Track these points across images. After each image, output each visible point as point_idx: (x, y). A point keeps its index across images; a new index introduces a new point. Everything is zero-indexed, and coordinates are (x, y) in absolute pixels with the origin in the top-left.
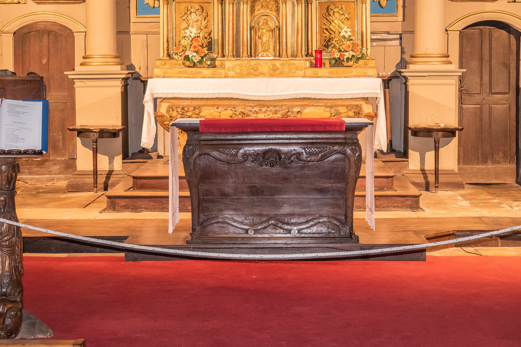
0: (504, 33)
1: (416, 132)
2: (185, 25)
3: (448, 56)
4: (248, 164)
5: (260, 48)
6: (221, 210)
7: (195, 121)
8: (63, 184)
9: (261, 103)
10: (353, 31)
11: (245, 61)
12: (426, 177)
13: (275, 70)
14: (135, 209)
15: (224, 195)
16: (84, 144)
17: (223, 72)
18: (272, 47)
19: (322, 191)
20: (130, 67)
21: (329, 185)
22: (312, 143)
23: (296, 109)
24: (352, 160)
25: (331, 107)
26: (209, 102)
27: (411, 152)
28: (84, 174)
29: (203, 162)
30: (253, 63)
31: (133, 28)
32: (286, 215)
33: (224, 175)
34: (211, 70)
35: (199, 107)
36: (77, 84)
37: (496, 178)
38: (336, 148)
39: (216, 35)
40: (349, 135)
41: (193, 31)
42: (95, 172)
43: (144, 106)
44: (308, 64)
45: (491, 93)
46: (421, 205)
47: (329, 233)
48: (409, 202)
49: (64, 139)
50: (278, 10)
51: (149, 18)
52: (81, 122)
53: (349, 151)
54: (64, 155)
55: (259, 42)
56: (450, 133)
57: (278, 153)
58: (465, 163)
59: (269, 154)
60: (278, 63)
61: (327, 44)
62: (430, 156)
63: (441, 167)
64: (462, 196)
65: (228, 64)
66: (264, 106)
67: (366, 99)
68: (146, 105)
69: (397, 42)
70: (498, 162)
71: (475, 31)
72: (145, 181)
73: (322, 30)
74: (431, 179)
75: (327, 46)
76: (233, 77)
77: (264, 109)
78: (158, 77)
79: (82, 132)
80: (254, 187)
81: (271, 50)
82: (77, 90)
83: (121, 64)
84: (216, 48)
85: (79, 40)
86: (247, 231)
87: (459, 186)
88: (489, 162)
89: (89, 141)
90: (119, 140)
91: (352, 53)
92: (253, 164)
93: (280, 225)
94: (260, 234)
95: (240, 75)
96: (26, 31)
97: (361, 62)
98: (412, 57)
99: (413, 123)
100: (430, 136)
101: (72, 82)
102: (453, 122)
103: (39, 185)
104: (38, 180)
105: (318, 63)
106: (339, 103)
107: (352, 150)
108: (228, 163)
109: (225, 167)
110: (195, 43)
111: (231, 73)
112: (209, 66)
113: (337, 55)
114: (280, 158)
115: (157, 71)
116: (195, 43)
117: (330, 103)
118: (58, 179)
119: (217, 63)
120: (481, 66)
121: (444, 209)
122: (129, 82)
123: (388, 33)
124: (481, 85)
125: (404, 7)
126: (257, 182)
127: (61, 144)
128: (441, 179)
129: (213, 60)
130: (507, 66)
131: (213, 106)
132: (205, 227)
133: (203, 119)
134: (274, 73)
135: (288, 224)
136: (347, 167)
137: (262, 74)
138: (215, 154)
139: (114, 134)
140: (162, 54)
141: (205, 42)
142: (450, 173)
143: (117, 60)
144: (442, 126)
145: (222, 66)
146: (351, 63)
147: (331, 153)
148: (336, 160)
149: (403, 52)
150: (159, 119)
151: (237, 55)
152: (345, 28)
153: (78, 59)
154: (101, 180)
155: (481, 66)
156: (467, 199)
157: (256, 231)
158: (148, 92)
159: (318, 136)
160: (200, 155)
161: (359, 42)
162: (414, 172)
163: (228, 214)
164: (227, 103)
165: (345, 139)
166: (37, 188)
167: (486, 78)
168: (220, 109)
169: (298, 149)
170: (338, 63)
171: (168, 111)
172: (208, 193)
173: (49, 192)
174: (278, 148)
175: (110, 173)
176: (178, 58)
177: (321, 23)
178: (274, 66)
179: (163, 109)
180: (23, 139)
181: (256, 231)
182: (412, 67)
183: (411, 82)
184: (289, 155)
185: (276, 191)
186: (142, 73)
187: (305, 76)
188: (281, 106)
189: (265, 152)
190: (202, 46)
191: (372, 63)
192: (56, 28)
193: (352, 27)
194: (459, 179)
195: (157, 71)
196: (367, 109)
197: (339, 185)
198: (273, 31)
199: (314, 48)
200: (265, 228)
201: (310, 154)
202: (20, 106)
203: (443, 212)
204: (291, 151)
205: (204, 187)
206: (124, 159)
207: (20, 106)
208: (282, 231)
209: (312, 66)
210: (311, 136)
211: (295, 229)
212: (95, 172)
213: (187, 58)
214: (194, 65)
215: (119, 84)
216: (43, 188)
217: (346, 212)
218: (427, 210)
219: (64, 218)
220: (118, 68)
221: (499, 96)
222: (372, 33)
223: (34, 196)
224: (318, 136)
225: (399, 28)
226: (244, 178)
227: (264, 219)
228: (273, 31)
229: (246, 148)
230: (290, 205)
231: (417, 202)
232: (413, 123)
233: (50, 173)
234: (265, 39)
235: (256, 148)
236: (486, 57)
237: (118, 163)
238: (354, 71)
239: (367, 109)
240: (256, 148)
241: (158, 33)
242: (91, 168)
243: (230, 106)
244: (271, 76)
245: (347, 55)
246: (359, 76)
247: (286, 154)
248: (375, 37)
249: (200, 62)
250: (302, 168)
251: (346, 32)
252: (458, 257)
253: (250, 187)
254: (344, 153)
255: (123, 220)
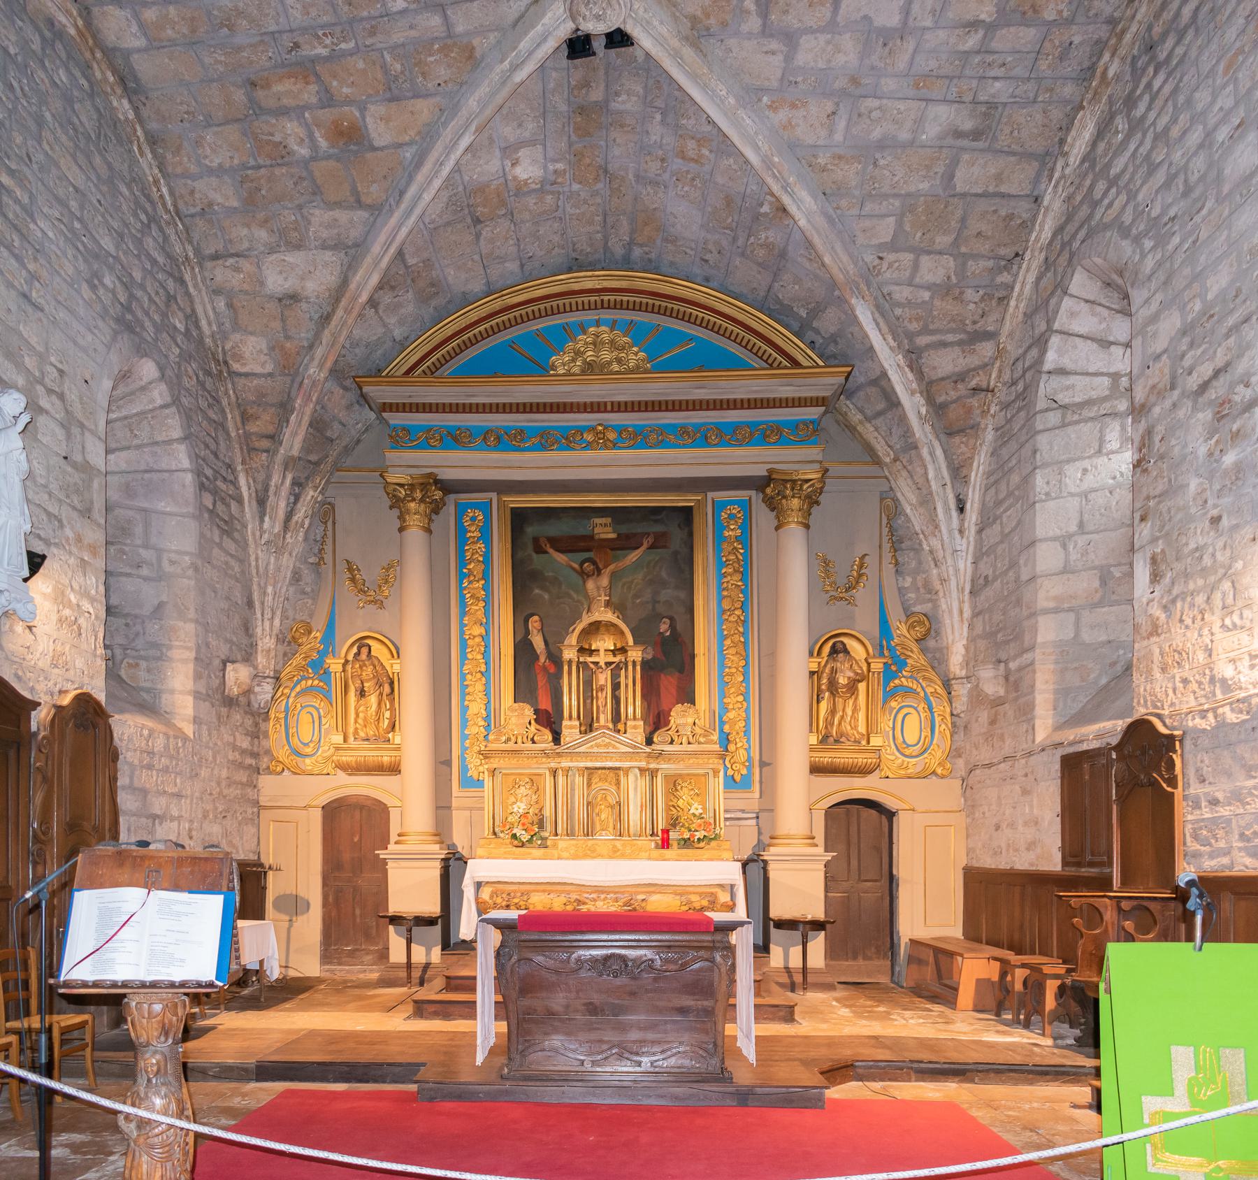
0: (873, 812)
1: (781, 924)
2: (512, 799)
3: (813, 838)
4: (583, 974)
5: (598, 827)
6: (546, 1034)
7: (513, 914)
8: (375, 976)
9: (600, 890)
10: (704, 809)
11: (581, 840)
12: (790, 977)
13: (615, 852)
14: (447, 1016)
15: (551, 1013)
16: (397, 933)
17: (555, 853)
18: (611, 825)
19: (682, 1011)
20: (451, 846)
21: (692, 1003)
22: (669, 947)
23: (641, 897)
24: (723, 970)
25: (681, 895)
26: (539, 887)
27: (772, 946)
28: (396, 966)
29: (523, 969)
30: (590, 843)
31: (455, 803)
32: (634, 1042)
33: (551, 987)
34: (543, 850)
35: (528, 893)
36: (390, 865)
37: (869, 976)
38: (702, 953)
39: (548, 812)
40: (718, 937)
41: (520, 807)
42: (409, 965)
43: (462, 892)
44: (653, 845)
45: (860, 880)
46: (796, 1017)
47: (693, 1067)
48: (781, 1014)
49: (377, 925)
50: (618, 783)
51: (472, 792)
52: (394, 907)
53: (718, 958)
54: (377, 944)
55: (597, 819)
56: (817, 925)
57: (623, 959)
58: (832, 959)
59: (612, 961)
60: (618, 844)
61: (674, 823)
62: (796, 951)
63: (810, 964)
64: (837, 1000)
65: (562, 844)
66: (603, 892)
67: (721, 886)
68: (465, 890)
69: (754, 822)
70: (870, 959)
71: (841, 810)
72: (459, 982)
73: (668, 808)
74: (798, 978)
75: (674, 825)
76: (567, 859)
77: (603, 896)
78: (481, 857)
79: (395, 920)
80: (591, 1003)
81: (611, 829)
82: (390, 872)
83: (441, 842)
84: (549, 826)
85: (394, 816)
86: (582, 1062)
87: (829, 987)
88: (860, 958)
89: (403, 929)
90: (437, 929)
91: (704, 833)
92: (590, 974)
93: (626, 1055)
94: (599, 1066)
95: (575, 857)
96: (335, 805)
97: (713, 843)
98: (772, 838)
99: (776, 912)
100: (796, 929)
101: (384, 862)
102: (819, 913)
103: (349, 977)
104: (348, 972)
105: (665, 844)
106: (691, 889)
107: (723, 957)
108: (557, 972)
109: (554, 978)
110: (523, 820)
111: (565, 854)
112: (540, 846)
113: (686, 835)
114: (627, 966)
115: (480, 852)
116: (523, 820)
117: (680, 890)
118: (371, 971)
119: (549, 843)
120: (849, 850)
121: (825, 1021)
122: (451, 862)
123: (743, 811)
124: (849, 871)
125: (761, 782)
126: (597, 998)
127: (374, 932)
128: (810, 979)
129: (544, 839)
130: (878, 850)
131: (544, 891)
132: (524, 1056)
133: (523, 912)
134: (614, 854)
135: (637, 1054)
136: (716, 979)
137: (601, 856)
138: (539, 959)
139: (430, 922)
140: (487, 832)
141: (536, 819)
142: (817, 971)
143: (437, 838)
144: (809, 917)
145: (555, 846)
146: (702, 844)
147: (694, 960)
148: (700, 970)
149: (760, 833)
150: (482, 908)
151: (570, 833)
152: (696, 805)
153: (393, 837)
154: (416, 974)
155: (849, 850)
156: (847, 1006)
157: (594, 1063)
158: (467, 875)
159: (677, 938)
160: (519, 960)
161: (712, 821)
162: (777, 970)
163: (556, 1041)
164: (559, 887)
165: (713, 941)
166: (345, 981)
167: (854, 863)
168: (552, 896)
169: (649, 954)
170: (686, 843)
171: (491, 897)
172: (529, 1011)
173: (356, 987)
174: (623, 952)
175: (427, 966)
176: (506, 837)
177: (667, 800)
178: (614, 846)
179: (485, 894)
180: (182, 961)
181: (594, 1063)
182: (773, 850)
183: (771, 867)
184: (638, 962)
185: (618, 1010)
186: (465, 853)
187: (649, 859)
188: (623, 893)
189: (607, 958)
190: (532, 824)
191: (727, 845)
192: (369, 803)
193: (703, 804)
194: (829, 979)
195: (480, 852)
196: (724, 897)
197: (706, 1003)
198: (612, 807)
199: (660, 827)
200: (606, 1058)
201: (666, 961)
202: (182, 903)
203: (824, 1026)
204: (641, 957)
205: (526, 1002)
206: (443, 950)
207: (182, 903)
208: (629, 1063)
209: (657, 847)
210: (667, 937)
211: (645, 1060)
212: (409, 965)
213: (514, 836)
214: (523, 845)
215: (438, 865)
216: (352, 981)
217: (716, 1039)
218: (805, 1023)
219: (359, 1028)
220: (437, 847)
221: (869, 884)
222: (726, 811)
223: (338, 991)
224: (677, 938)
225: (755, 806)
226: (577, 992)
227: (605, 1047)
228: (612, 807)
229: (581, 952)
230: (640, 1029)
231: (792, 1013)
232: (776, 912)
233: (362, 963)
234: (603, 816)
235: (595, 952)
236: (854, 839)
237: (436, 955)
238: (706, 853)
239: (724, 897)
240: (595, 952)
241: (483, 809)
242: (405, 961)
243: (563, 892)
244: (611, 857)
245: (698, 835)
246: (712, 860)
247: (634, 960)
248: (728, 816)
249: (530, 841)
250: (655, 979)
251: (696, 809)
252: (866, 1102)
253: (585, 1004)
254: (712, 961)
255: (428, 1033)
